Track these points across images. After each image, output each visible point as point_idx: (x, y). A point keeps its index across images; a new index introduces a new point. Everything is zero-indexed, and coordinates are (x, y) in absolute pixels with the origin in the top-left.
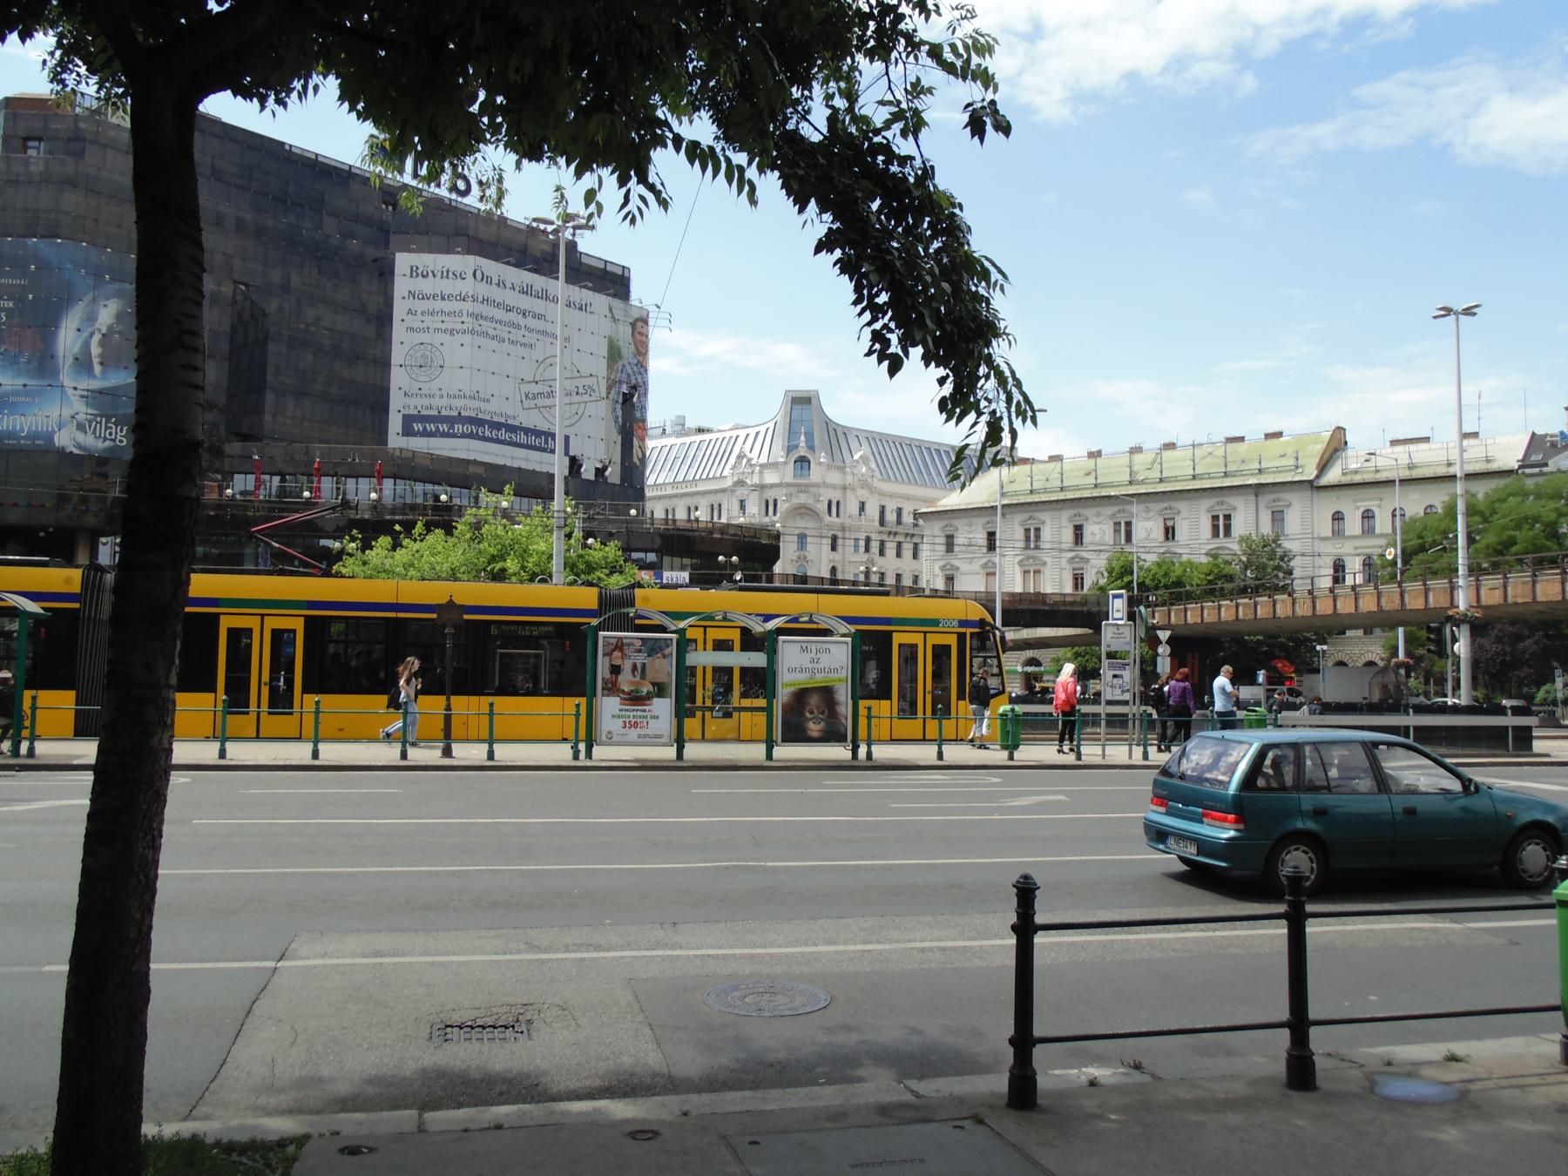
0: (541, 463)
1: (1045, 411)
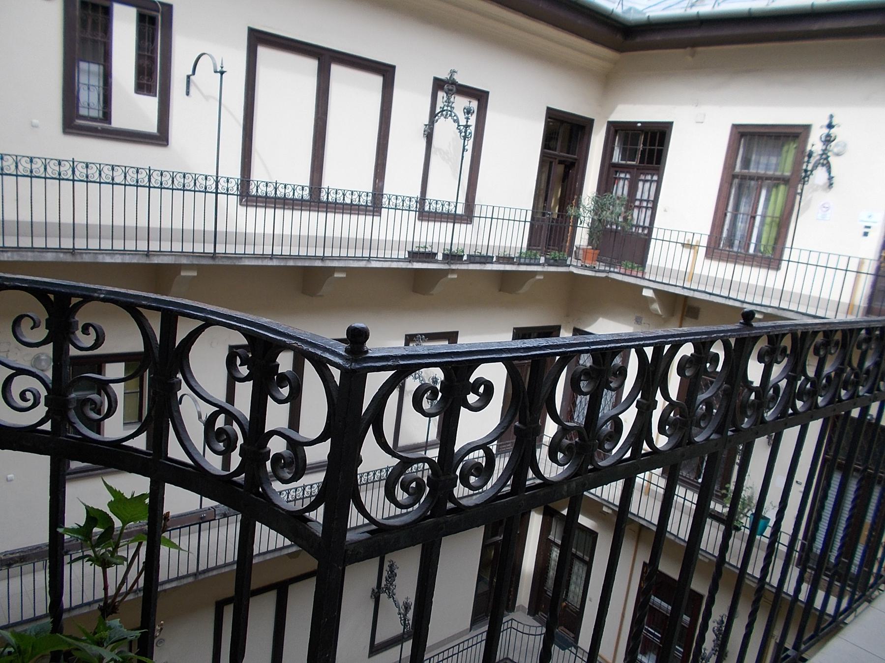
0: (525, 222)
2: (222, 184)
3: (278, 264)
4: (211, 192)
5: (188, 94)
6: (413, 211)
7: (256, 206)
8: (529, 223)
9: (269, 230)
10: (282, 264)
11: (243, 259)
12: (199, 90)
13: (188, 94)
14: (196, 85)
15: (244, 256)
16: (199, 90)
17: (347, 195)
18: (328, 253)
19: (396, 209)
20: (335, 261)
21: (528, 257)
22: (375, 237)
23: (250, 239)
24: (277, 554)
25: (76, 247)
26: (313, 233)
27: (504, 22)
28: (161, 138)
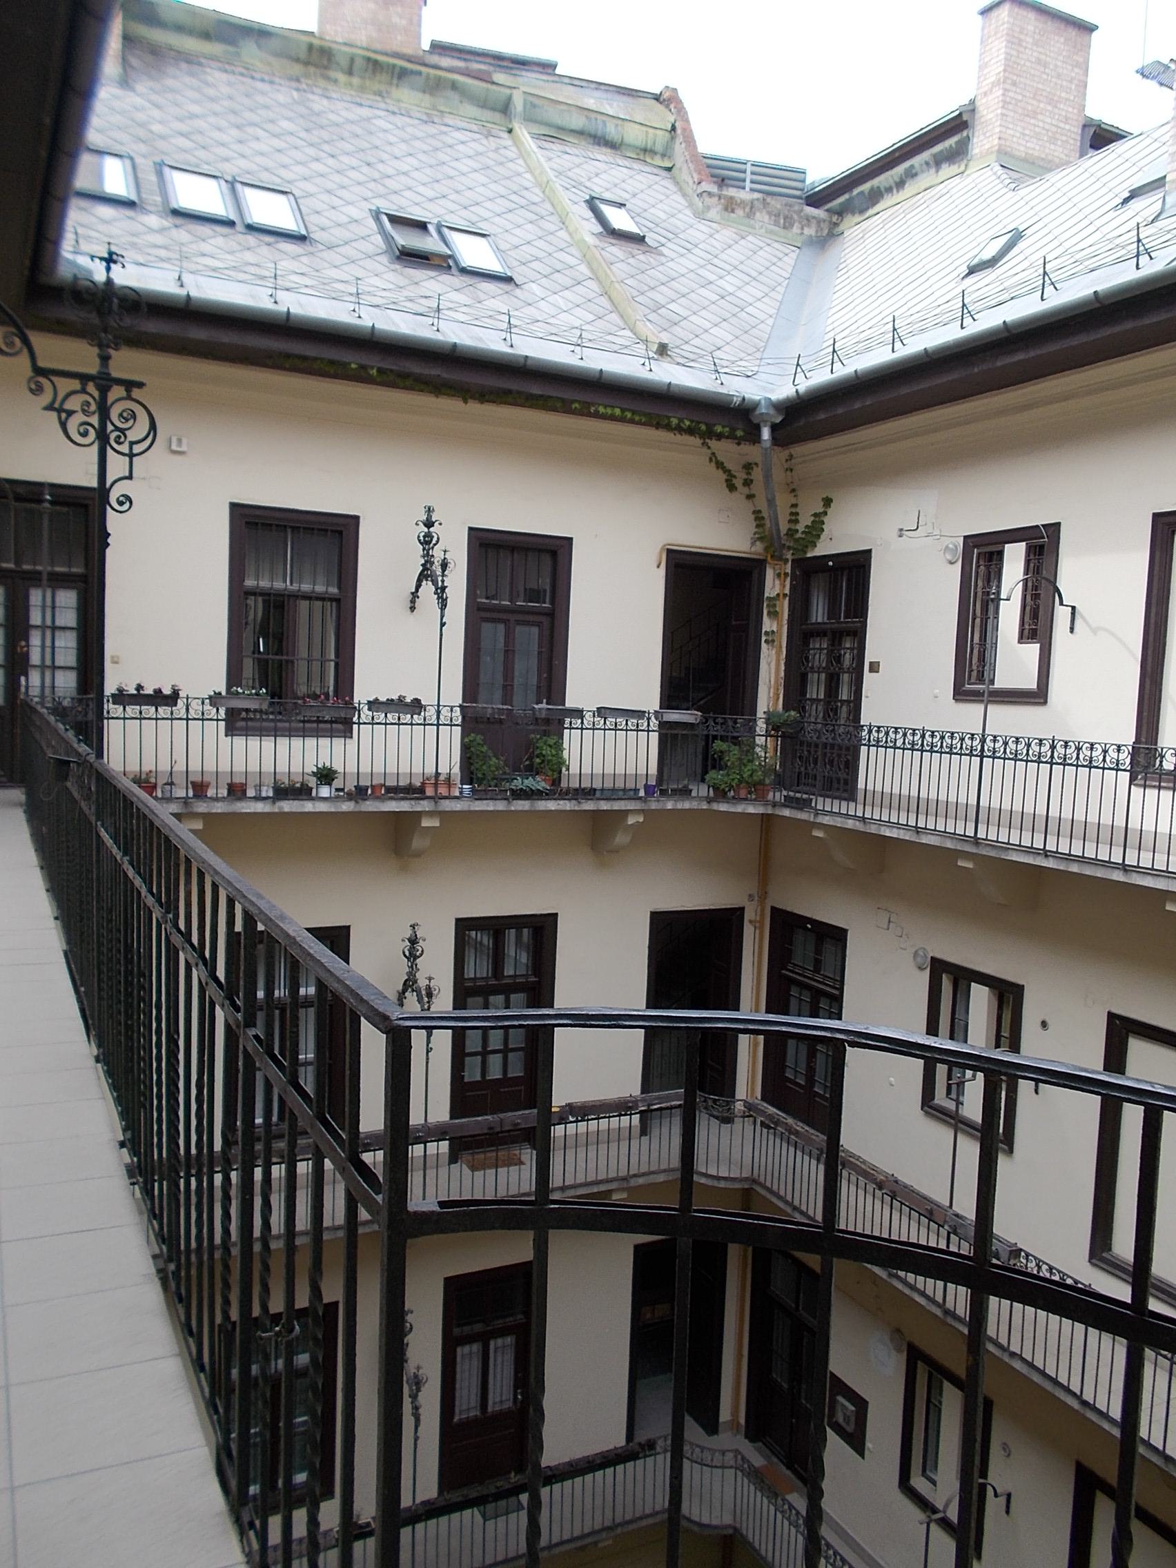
1: (1008, 1512)
2: (445, 712)
3: (1055, 867)
4: (1125, 770)
5: (1072, 630)
6: (577, 728)
7: (1160, 788)
8: (657, 734)
9: (1041, 810)
10: (1061, 868)
11: (1010, 852)
12: (1087, 623)
13: (1072, 630)
14: (1083, 617)
15: (1008, 847)
16: (1087, 623)
17: (1110, 751)
18: (1131, 860)
19: (1117, 770)
20: (1149, 878)
21: (661, 786)
22: (1054, 813)
23: (1148, 841)
24: (1048, 1386)
25: (1126, 863)
26: (1106, 820)
27: (1131, 382)
28: (1038, 696)
